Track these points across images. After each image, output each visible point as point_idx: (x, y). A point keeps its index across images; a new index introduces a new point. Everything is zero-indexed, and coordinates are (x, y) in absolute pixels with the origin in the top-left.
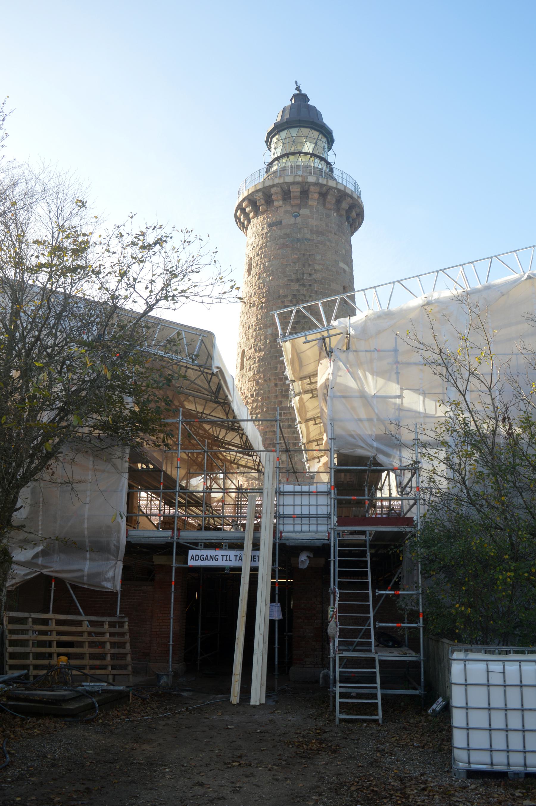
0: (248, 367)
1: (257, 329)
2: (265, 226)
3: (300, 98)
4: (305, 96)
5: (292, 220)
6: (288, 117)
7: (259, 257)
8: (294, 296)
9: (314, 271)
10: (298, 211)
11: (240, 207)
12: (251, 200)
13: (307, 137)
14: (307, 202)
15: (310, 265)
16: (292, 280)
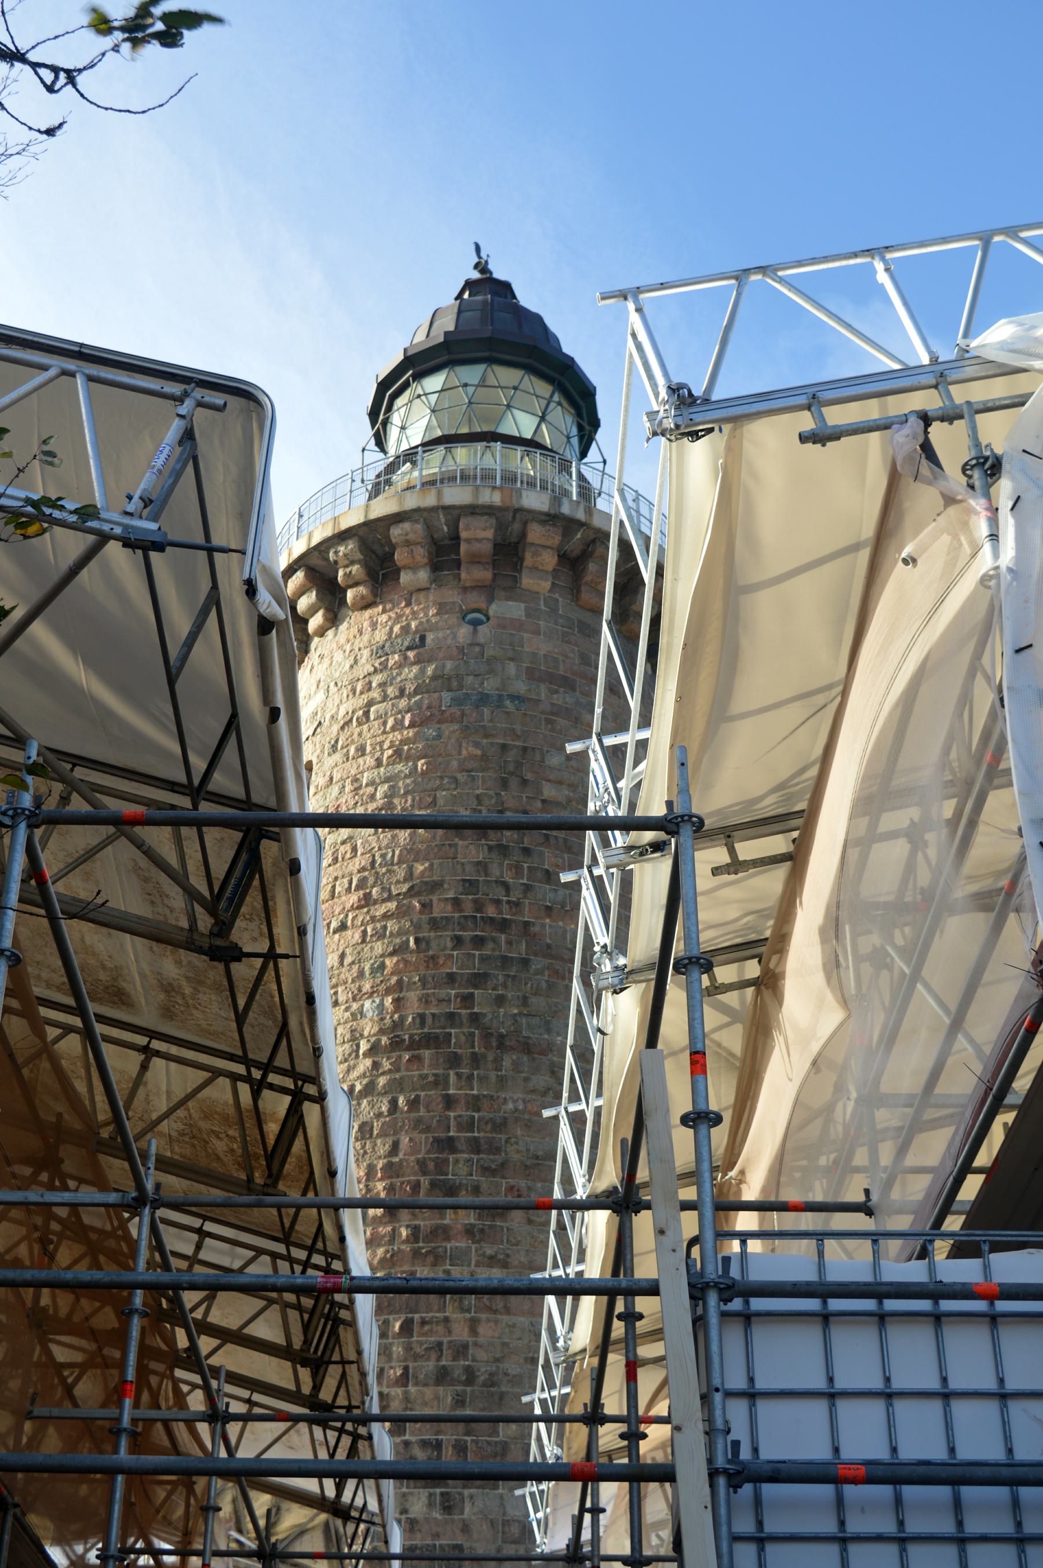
2: (366, 653)
3: (488, 291)
5: (464, 632)
6: (451, 328)
7: (338, 757)
8: (470, 886)
9: (539, 805)
10: (484, 606)
13: (515, 388)
14: (516, 580)
15: (524, 782)
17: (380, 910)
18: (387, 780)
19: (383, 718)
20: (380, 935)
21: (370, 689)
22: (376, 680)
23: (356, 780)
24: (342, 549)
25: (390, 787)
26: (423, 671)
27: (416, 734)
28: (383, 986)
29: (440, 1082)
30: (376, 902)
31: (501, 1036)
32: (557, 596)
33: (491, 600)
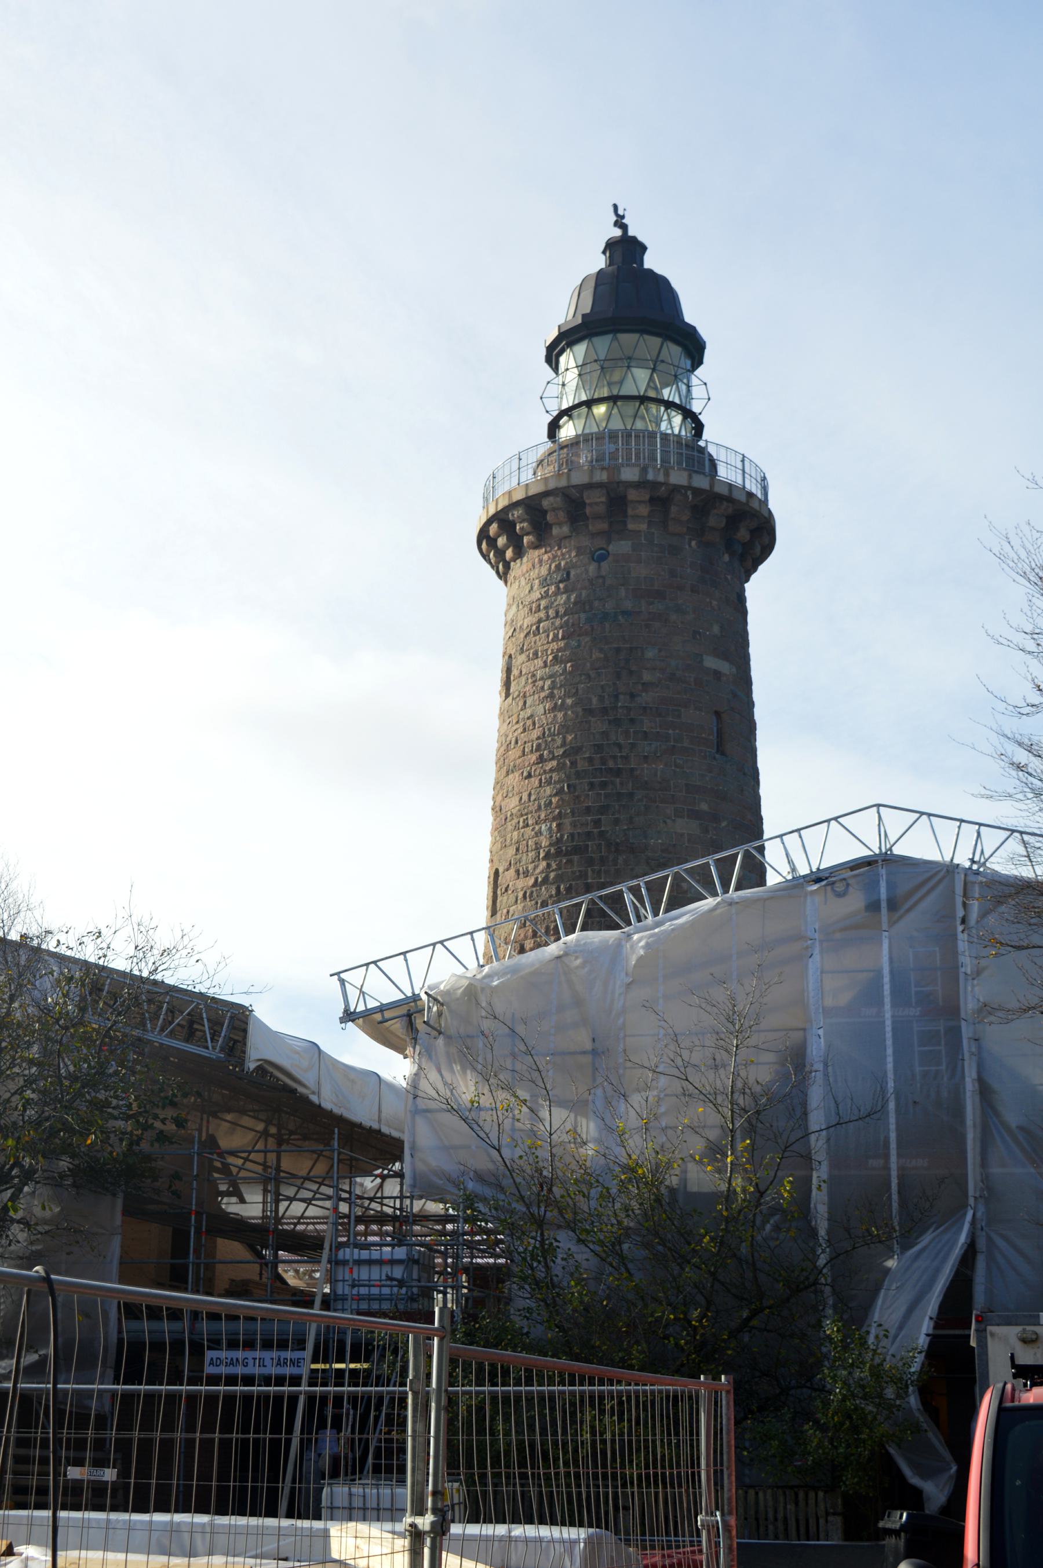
0: (505, 911)
1: (521, 824)
2: (537, 581)
3: (625, 250)
4: (634, 239)
5: (592, 568)
8: (599, 748)
9: (640, 687)
10: (605, 546)
11: (483, 535)
12: (502, 520)
15: (631, 673)
16: (589, 712)
17: (549, 766)
18: (550, 677)
19: (546, 631)
20: (549, 782)
21: (539, 610)
22: (543, 603)
23: (534, 675)
24: (516, 513)
25: (553, 682)
26: (568, 598)
27: (566, 645)
28: (551, 816)
29: (583, 875)
30: (546, 761)
31: (617, 844)
32: (653, 530)
33: (609, 543)
